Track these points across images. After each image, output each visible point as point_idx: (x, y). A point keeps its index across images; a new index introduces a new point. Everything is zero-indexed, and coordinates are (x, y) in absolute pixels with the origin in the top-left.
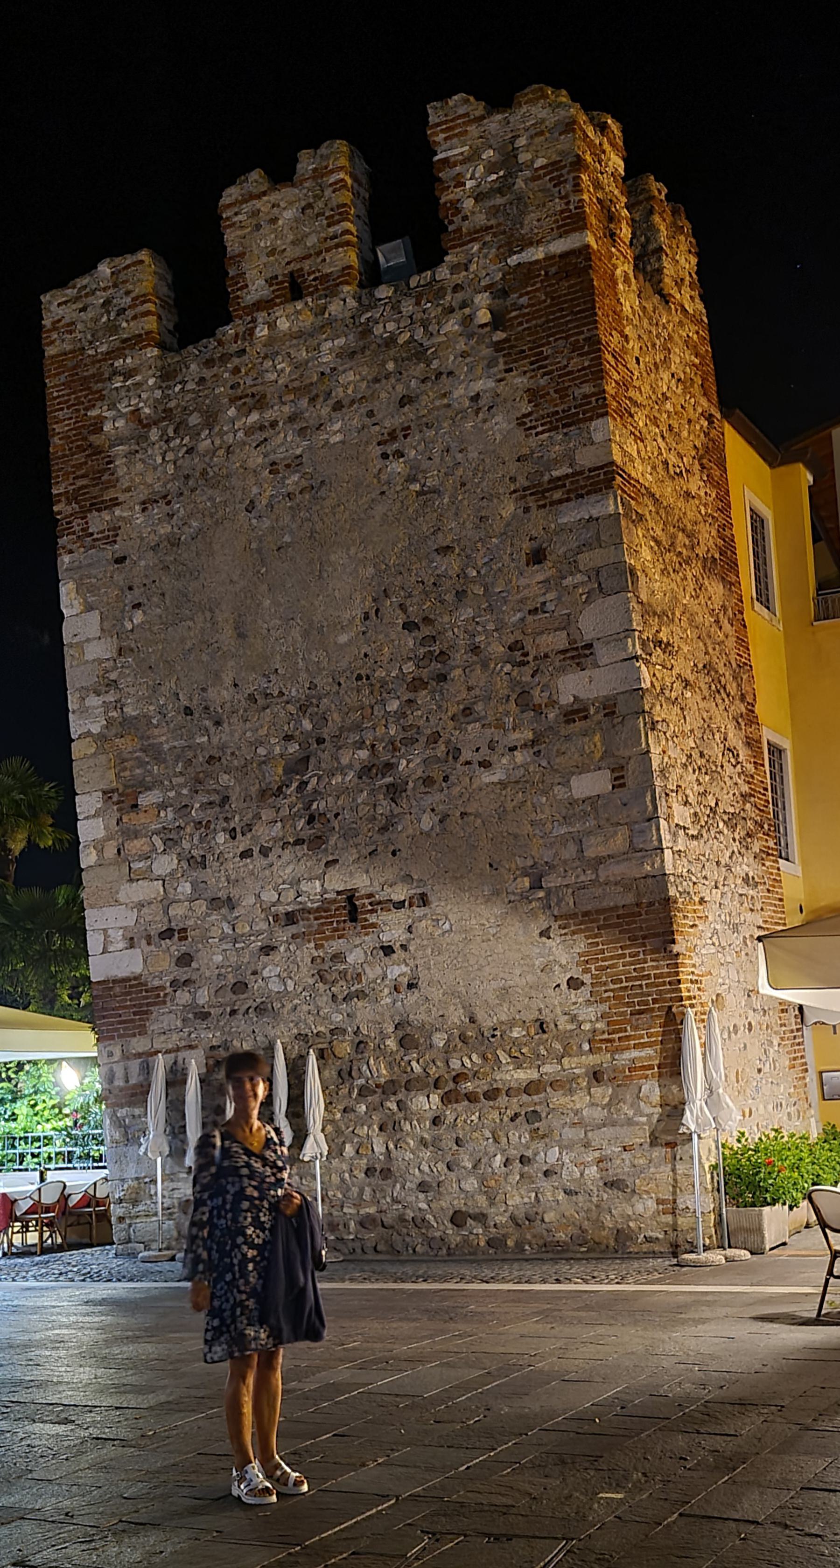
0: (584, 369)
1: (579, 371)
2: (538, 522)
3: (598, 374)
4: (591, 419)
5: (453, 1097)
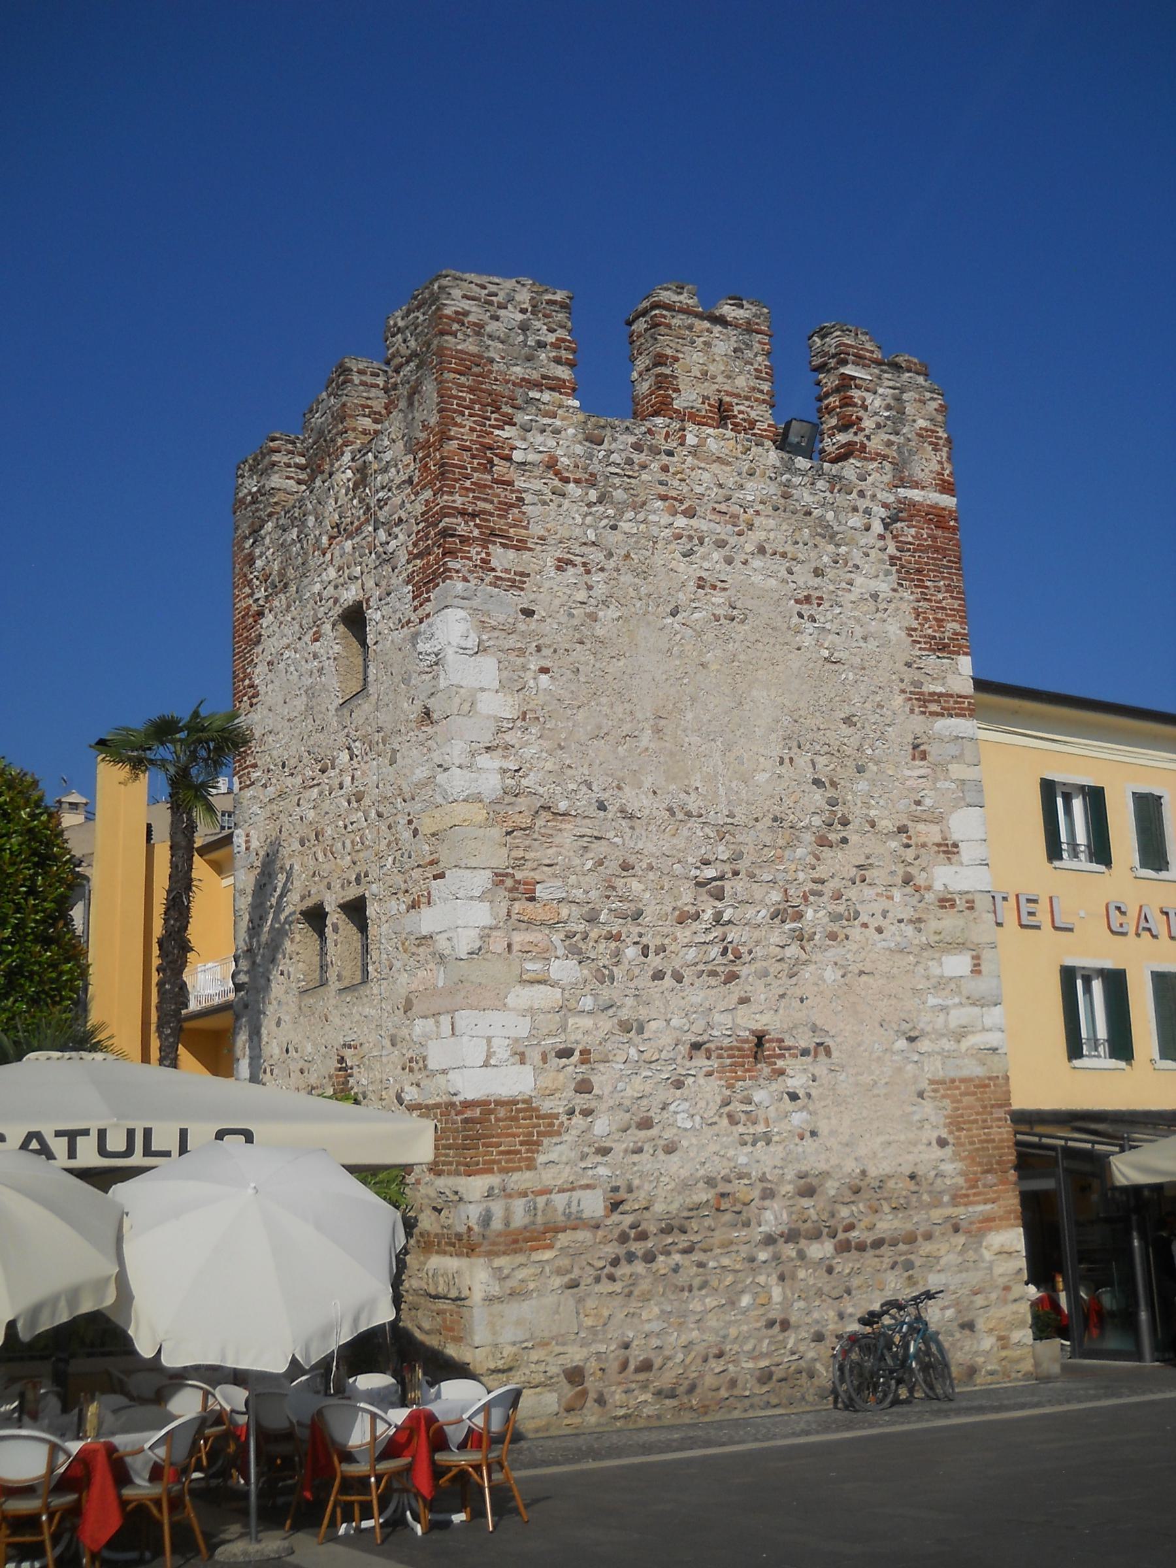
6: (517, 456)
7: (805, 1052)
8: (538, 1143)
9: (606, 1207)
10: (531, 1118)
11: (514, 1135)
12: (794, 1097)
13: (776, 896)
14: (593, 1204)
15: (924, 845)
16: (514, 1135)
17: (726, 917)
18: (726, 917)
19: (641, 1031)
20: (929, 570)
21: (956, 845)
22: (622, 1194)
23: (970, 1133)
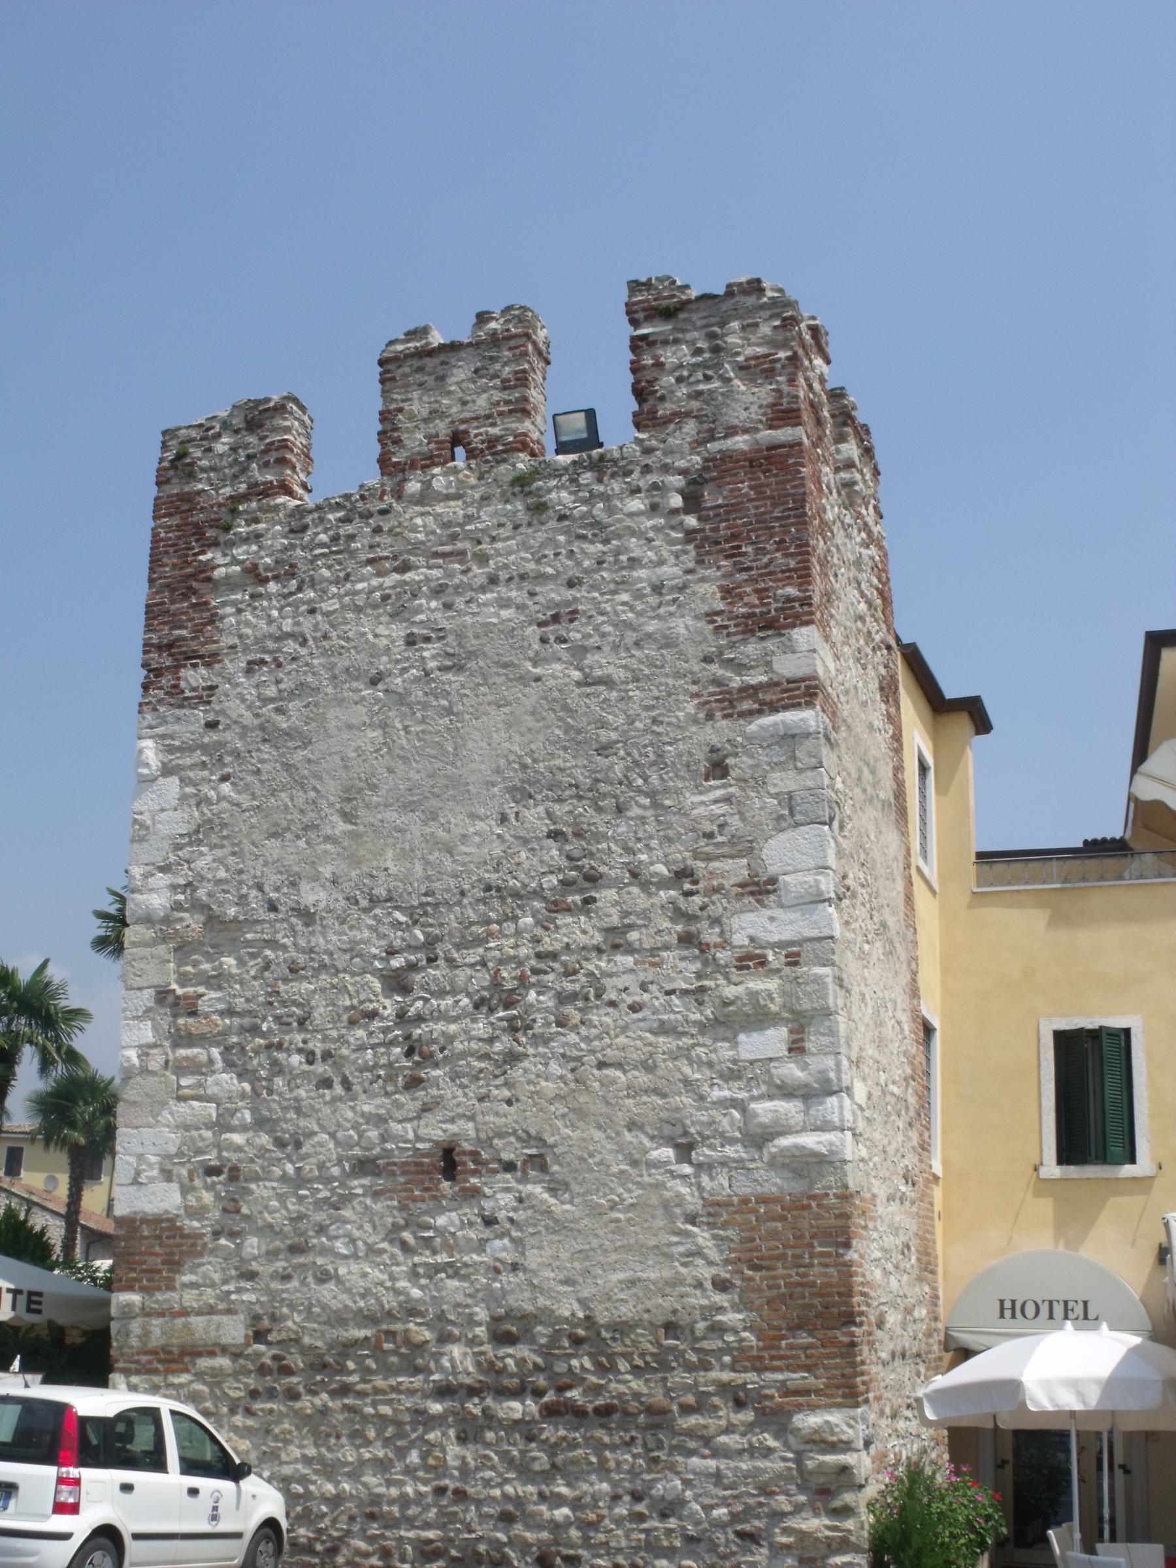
0: (789, 570)
1: (783, 572)
2: (720, 731)
3: (803, 576)
4: (793, 626)
5: (369, 1167)
6: (219, 573)
7: (509, 1167)
8: (179, 1264)
9: (247, 1336)
10: (174, 1237)
11: (156, 1254)
12: (489, 1222)
13: (483, 978)
14: (234, 1330)
15: (716, 890)
16: (156, 1254)
17: (412, 1011)
18: (412, 1011)
19: (298, 1145)
20: (749, 531)
21: (773, 881)
22: (266, 1323)
23: (772, 1273)
